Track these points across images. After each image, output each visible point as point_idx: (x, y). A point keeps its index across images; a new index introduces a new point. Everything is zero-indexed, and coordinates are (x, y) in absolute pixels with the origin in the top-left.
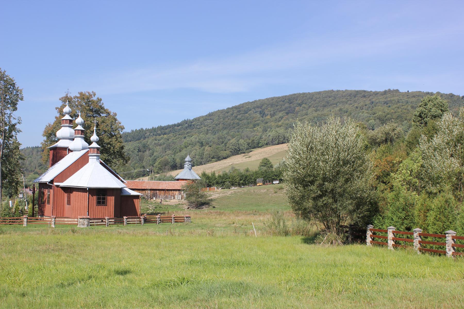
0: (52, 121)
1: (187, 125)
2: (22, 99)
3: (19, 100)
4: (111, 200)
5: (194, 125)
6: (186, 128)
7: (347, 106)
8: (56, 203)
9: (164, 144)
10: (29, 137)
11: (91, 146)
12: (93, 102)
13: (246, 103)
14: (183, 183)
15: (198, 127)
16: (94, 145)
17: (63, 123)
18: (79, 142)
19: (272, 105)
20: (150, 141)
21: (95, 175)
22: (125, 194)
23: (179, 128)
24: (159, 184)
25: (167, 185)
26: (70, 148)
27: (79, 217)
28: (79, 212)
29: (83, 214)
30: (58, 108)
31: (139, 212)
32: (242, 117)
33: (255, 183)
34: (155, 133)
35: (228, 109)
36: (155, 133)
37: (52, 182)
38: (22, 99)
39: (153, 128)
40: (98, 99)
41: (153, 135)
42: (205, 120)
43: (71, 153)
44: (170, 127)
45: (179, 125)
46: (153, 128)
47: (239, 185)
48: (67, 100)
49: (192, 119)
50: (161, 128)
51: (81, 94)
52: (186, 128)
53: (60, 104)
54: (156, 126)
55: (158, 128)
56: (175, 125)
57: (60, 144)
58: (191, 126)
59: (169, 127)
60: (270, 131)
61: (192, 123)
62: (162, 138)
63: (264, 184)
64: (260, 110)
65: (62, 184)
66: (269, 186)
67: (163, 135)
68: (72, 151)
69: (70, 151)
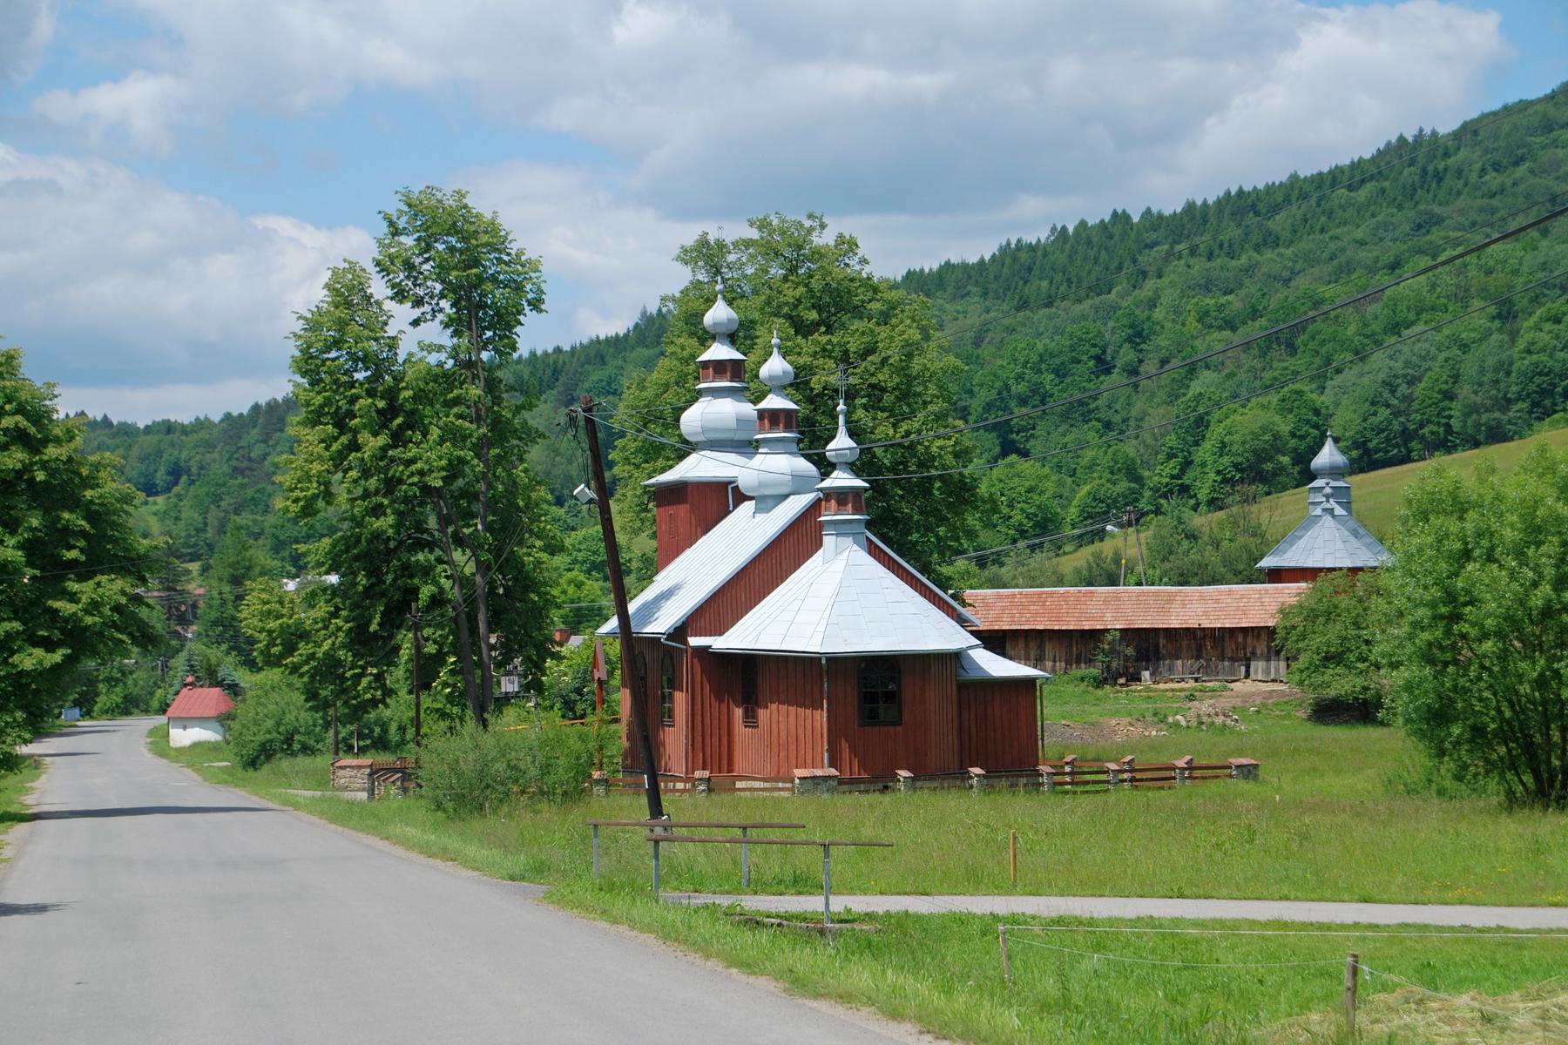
2: (536, 305)
3: (527, 309)
5: (1460, 173)
8: (699, 718)
9: (1255, 314)
11: (827, 483)
12: (818, 254)
14: (1290, 592)
16: (841, 479)
20: (1169, 297)
21: (846, 604)
22: (973, 675)
23: (1363, 194)
24: (1170, 601)
25: (1211, 604)
26: (743, 484)
27: (799, 772)
29: (809, 761)
31: (1050, 745)
34: (1204, 241)
38: (536, 305)
41: (1193, 252)
43: (748, 506)
44: (1287, 200)
57: (698, 467)
59: (1295, 191)
61: (1446, 155)
62: (1249, 270)
65: (719, 643)
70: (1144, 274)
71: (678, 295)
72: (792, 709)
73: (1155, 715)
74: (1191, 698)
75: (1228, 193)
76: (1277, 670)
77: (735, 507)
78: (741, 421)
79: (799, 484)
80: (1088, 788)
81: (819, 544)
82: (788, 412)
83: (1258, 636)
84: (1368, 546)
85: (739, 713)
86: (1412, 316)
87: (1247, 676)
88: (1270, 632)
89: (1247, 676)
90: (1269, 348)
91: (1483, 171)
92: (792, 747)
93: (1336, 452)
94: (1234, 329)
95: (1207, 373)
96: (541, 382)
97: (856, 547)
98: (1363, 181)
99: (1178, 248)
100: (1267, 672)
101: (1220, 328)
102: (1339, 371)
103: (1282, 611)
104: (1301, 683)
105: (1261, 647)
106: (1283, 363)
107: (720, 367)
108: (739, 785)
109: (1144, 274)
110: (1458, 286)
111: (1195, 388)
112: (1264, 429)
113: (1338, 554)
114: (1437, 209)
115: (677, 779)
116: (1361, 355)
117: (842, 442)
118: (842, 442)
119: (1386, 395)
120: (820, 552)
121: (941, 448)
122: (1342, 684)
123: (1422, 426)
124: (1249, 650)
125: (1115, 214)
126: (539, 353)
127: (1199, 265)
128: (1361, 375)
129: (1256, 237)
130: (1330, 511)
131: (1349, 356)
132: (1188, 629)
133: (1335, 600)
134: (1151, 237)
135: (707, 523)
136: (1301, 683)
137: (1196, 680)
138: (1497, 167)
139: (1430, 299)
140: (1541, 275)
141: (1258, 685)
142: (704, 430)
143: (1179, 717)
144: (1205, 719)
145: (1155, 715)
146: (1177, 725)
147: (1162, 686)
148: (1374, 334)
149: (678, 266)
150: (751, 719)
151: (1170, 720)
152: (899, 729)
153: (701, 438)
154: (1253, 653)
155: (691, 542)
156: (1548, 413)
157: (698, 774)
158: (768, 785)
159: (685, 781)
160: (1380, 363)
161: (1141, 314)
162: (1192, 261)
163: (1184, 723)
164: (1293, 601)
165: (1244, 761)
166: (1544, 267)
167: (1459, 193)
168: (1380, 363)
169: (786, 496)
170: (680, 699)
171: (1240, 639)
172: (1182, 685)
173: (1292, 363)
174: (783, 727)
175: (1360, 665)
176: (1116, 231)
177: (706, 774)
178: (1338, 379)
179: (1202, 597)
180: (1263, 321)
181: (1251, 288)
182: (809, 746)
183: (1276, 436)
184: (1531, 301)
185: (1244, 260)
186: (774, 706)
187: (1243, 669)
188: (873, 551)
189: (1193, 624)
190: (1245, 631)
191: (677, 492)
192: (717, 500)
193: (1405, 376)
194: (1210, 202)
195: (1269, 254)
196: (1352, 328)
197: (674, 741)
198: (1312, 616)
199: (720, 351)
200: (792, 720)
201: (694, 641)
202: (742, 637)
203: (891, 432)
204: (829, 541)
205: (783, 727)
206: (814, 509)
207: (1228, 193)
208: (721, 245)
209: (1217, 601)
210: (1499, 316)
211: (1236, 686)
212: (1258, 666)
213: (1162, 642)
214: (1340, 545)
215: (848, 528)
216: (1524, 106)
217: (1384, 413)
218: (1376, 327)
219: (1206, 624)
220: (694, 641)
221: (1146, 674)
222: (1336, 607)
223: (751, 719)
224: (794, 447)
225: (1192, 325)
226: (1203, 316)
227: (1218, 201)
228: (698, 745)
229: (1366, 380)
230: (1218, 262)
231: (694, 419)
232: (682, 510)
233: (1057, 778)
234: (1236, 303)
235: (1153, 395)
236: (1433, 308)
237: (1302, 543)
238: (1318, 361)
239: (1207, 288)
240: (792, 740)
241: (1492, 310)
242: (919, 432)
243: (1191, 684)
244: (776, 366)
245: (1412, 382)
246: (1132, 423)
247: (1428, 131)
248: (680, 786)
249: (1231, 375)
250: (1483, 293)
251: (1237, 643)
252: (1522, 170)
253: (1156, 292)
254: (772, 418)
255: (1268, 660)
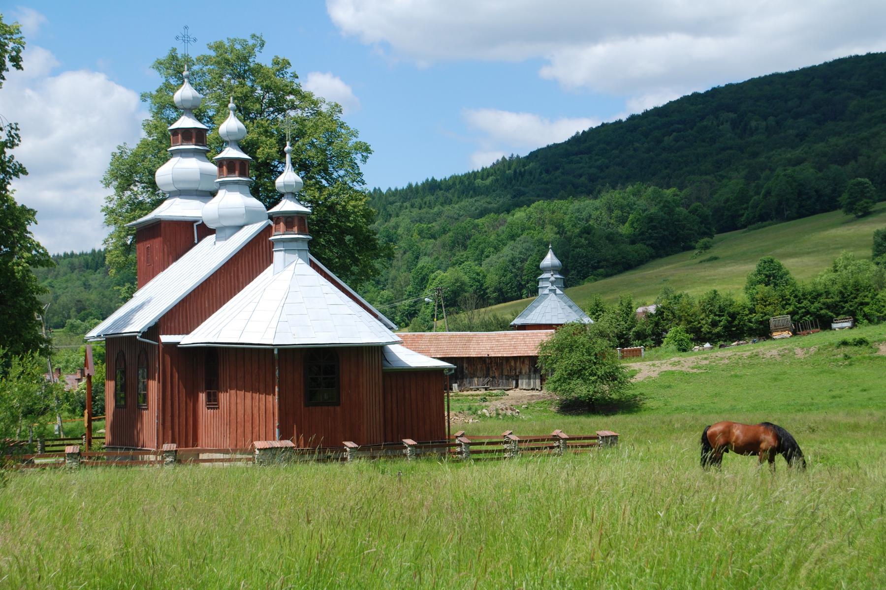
0: (135, 138)
4: (527, 362)
5: (531, 173)
8: (169, 402)
9: (444, 231)
10: (69, 216)
14: (544, 335)
17: (175, 143)
18: (234, 201)
21: (295, 306)
25: (494, 343)
27: (259, 444)
30: (151, 96)
32: (676, 140)
33: (764, 332)
37: (153, 331)
39: (410, 186)
43: (211, 239)
46: (410, 186)
47: (713, 339)
48: (176, 67)
50: (432, 186)
51: (218, 47)
53: (156, 80)
54: (418, 179)
57: (174, 209)
60: (768, 179)
61: (524, 166)
62: (439, 214)
63: (795, 333)
64: (732, 115)
65: (185, 340)
66: (817, 339)
67: (442, 204)
68: (212, 232)
69: (205, 231)
70: (390, 215)
71: (154, 93)
72: (249, 395)
73: (470, 409)
74: (485, 400)
75: (427, 180)
76: (534, 383)
77: (199, 240)
78: (204, 175)
79: (251, 217)
80: (481, 456)
81: (269, 261)
82: (242, 161)
83: (523, 363)
84: (575, 311)
85: (202, 397)
86: (520, 232)
87: (517, 386)
88: (533, 359)
89: (517, 386)
90: (453, 247)
91: (541, 174)
92: (248, 425)
93: (554, 258)
94: (435, 238)
95: (426, 257)
96: (97, 263)
97: (300, 261)
98: (488, 176)
99: (405, 204)
100: (529, 385)
101: (429, 238)
102: (487, 257)
103: (541, 345)
104: (555, 390)
105: (525, 369)
106: (460, 254)
107: (187, 134)
108: (202, 456)
109: (390, 215)
110: (540, 219)
111: (420, 265)
112: (457, 280)
113: (560, 316)
114: (522, 189)
115: (148, 452)
116: (497, 249)
117: (288, 177)
118: (288, 177)
119: (511, 267)
120: (272, 265)
121: (354, 207)
122: (580, 390)
123: (528, 283)
124: (518, 370)
125: (375, 189)
126: (97, 250)
127: (415, 212)
128: (498, 258)
129: (441, 200)
130: (554, 291)
131: (492, 249)
132: (481, 358)
133: (576, 338)
134: (392, 199)
135: (177, 254)
136: (555, 390)
137: (486, 389)
138: (547, 172)
139: (528, 224)
140: (577, 214)
141: (521, 393)
142: (174, 182)
143: (484, 411)
144: (500, 412)
145: (470, 409)
146: (484, 415)
147: (465, 393)
148: (502, 240)
149: (155, 73)
150: (213, 402)
151: (479, 412)
152: (338, 409)
153: (172, 188)
154: (521, 373)
155: (164, 266)
156: (585, 278)
157: (166, 447)
158: (227, 456)
159: (155, 453)
160: (507, 251)
161: (392, 231)
162: (412, 210)
163: (488, 415)
164: (549, 339)
165: (608, 433)
166: (578, 210)
167: (531, 182)
168: (507, 251)
169: (241, 227)
170: (154, 387)
171: (513, 364)
172: (478, 392)
173: (465, 254)
174: (240, 407)
175: (593, 378)
176: (377, 197)
177: (173, 447)
178: (488, 260)
179: (489, 338)
180: (451, 234)
181: (441, 221)
182: (263, 423)
183: (463, 283)
184: (573, 226)
185: (436, 209)
186: (233, 392)
187: (514, 382)
188: (313, 265)
189: (484, 354)
190: (515, 358)
191: (156, 228)
192: (187, 234)
193: (520, 258)
194: (419, 184)
195: (447, 207)
196: (493, 237)
197: (150, 421)
198: (560, 349)
199: (187, 122)
200: (248, 401)
201: (165, 339)
202: (205, 334)
203: (317, 195)
204: (278, 256)
205: (240, 407)
206: (266, 231)
207: (427, 180)
208: (188, 61)
209: (498, 341)
210: (558, 233)
211: (510, 392)
212: (523, 383)
213: (465, 365)
214: (561, 311)
215: (294, 245)
216: (556, 146)
217: (509, 275)
218: (503, 236)
219: (492, 355)
220: (165, 339)
221: (455, 386)
222: (576, 342)
223: (213, 402)
224: (247, 189)
225: (416, 236)
226: (420, 233)
227: (423, 184)
228: (168, 424)
229: (501, 260)
230: (424, 210)
231: (165, 174)
232: (156, 244)
233: (472, 448)
234: (436, 226)
235: (399, 268)
236: (529, 229)
237: (538, 309)
238: (478, 252)
239: (421, 220)
240: (248, 418)
241: (556, 229)
242: (338, 195)
243: (483, 392)
244: (231, 124)
245: (523, 261)
246: (390, 281)
247: (515, 156)
248: (152, 458)
249: (437, 258)
250: (551, 222)
251: (511, 366)
252: (558, 173)
253: (396, 223)
254: (230, 165)
255: (529, 378)
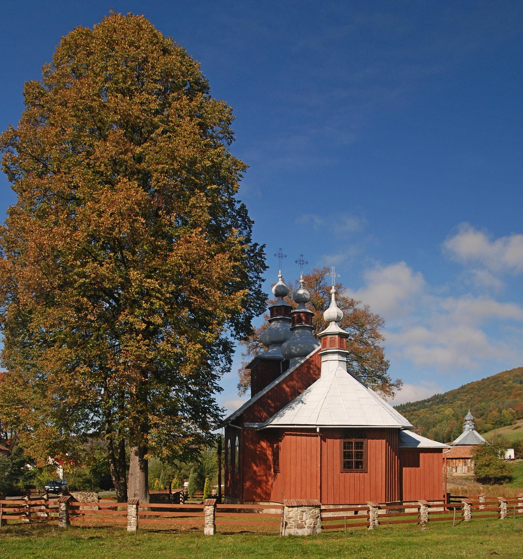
1: (438, 400)
6: (438, 403)
7: (483, 404)
13: (504, 373)
15: (451, 401)
19: (160, 500)
28: (299, 489)
32: (500, 387)
34: (404, 410)
35: (483, 380)
36: (404, 410)
40: (365, 306)
42: (459, 393)
45: (429, 400)
49: (442, 393)
52: (438, 403)
55: (407, 404)
56: (425, 401)
58: (442, 400)
59: (418, 403)
